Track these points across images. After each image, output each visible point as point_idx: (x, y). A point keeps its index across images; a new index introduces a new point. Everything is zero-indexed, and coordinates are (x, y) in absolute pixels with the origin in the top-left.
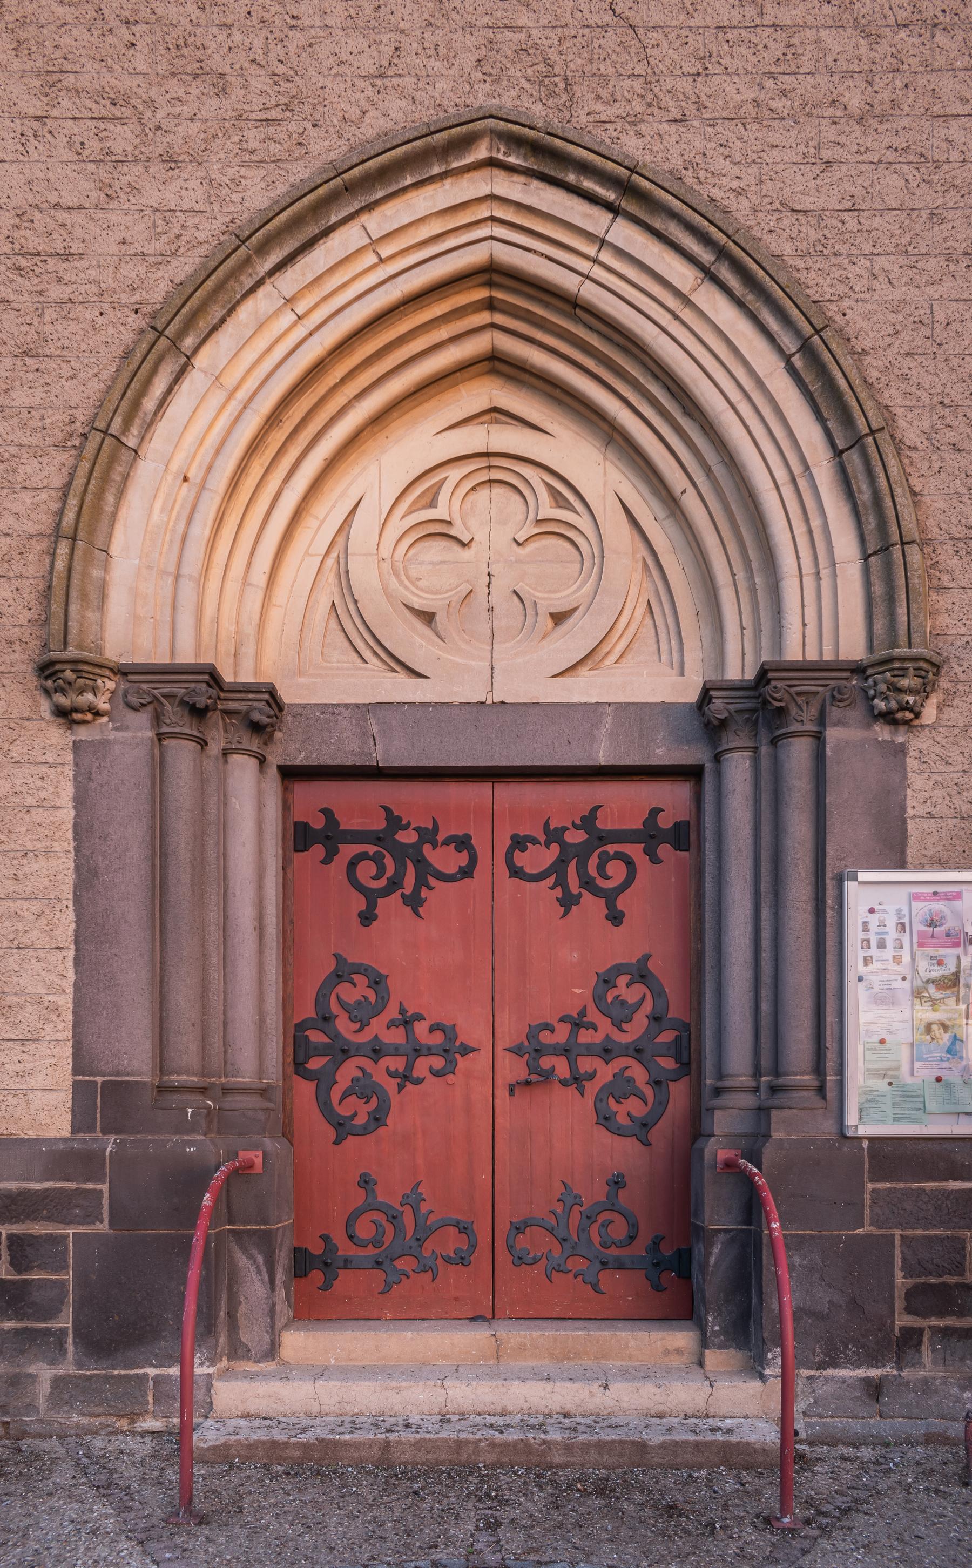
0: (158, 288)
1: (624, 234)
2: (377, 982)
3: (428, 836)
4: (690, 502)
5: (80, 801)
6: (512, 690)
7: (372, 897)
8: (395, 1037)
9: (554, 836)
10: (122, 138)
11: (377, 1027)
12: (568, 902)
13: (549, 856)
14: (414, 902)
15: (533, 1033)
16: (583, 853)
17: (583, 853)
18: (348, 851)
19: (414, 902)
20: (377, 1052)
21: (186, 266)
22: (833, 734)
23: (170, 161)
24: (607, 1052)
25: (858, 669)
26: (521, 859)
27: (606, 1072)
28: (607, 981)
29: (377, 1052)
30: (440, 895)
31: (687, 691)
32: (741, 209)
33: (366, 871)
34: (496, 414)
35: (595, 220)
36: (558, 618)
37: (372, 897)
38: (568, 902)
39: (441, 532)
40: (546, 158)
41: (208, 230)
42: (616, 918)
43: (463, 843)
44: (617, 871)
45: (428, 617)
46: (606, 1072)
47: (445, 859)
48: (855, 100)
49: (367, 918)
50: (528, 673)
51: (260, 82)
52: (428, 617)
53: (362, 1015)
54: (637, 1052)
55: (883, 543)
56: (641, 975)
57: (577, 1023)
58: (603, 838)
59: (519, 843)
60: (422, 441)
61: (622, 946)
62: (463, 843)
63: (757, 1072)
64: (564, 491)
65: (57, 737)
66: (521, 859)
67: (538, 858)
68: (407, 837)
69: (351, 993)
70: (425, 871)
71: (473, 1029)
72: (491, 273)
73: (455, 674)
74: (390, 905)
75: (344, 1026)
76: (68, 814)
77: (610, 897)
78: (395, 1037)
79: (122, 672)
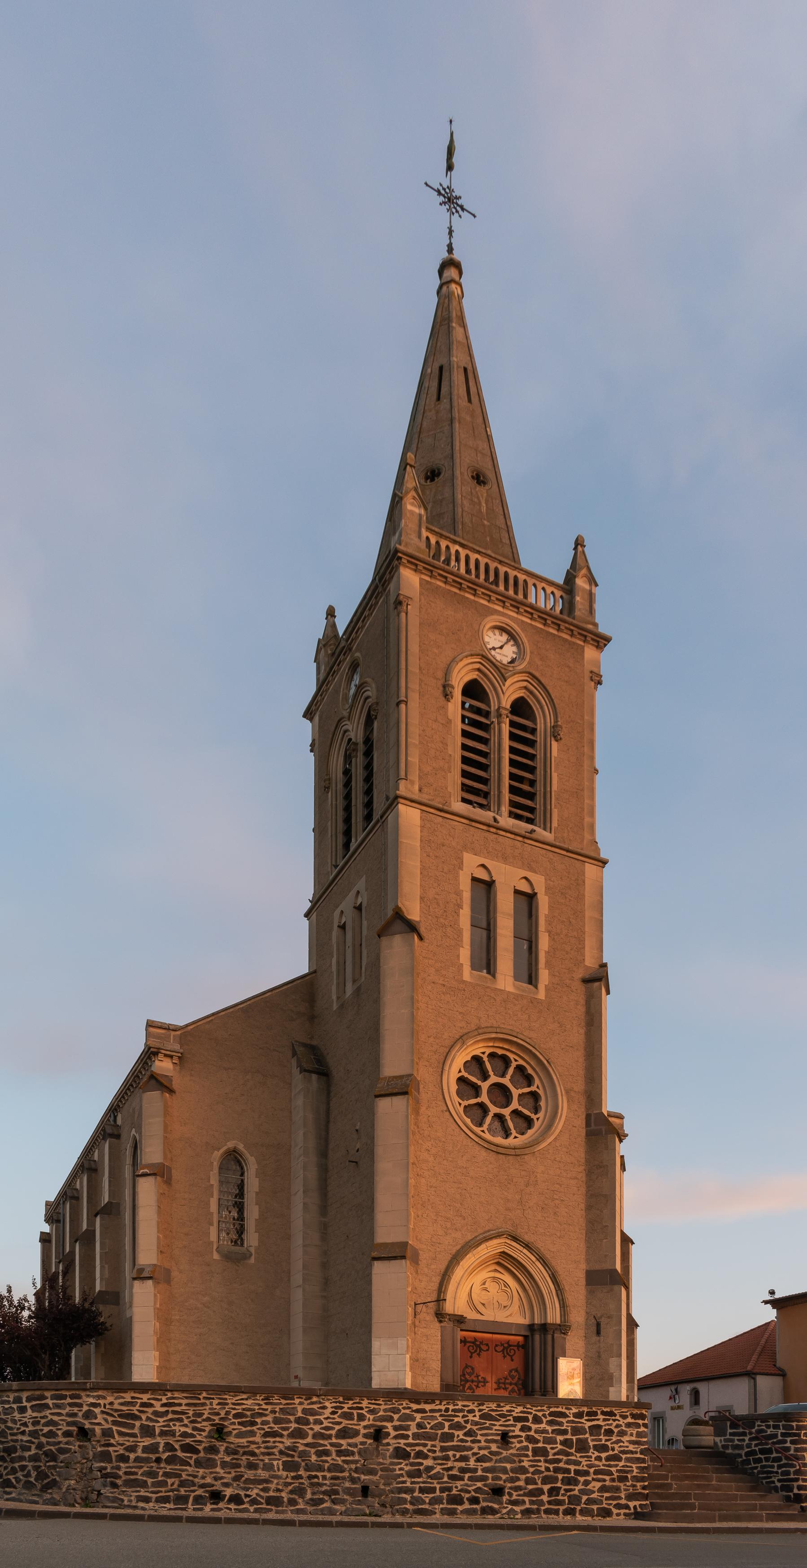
0: (454, 1251)
1: (525, 1251)
2: (473, 1369)
3: (481, 1343)
4: (530, 1291)
5: (441, 1336)
6: (498, 1319)
7: (472, 1353)
8: (475, 1379)
9: (502, 1345)
10: (449, 1225)
11: (473, 1377)
12: (504, 1357)
13: (502, 1348)
14: (479, 1355)
15: (498, 1380)
16: (507, 1348)
17: (507, 1348)
18: (468, 1344)
19: (479, 1355)
20: (472, 1381)
21: (459, 1247)
22: (556, 1335)
23: (456, 1230)
24: (511, 1384)
25: (560, 1325)
26: (497, 1348)
27: (510, 1388)
28: (511, 1371)
29: (472, 1381)
30: (483, 1354)
31: (526, 1321)
32: (542, 1249)
33: (471, 1348)
34: (496, 1271)
35: (521, 1248)
36: (505, 1307)
37: (472, 1353)
38: (504, 1357)
39: (486, 1289)
40: (515, 1239)
41: (462, 1242)
42: (512, 1360)
43: (487, 1345)
44: (512, 1352)
45: (483, 1304)
46: (510, 1388)
47: (484, 1347)
48: (558, 1234)
49: (471, 1357)
50: (501, 1317)
51: (470, 1219)
52: (483, 1304)
53: (470, 1374)
54: (516, 1384)
55: (563, 1306)
56: (516, 1371)
57: (506, 1379)
58: (510, 1346)
59: (497, 1346)
60: (485, 1274)
61: (514, 1365)
62: (487, 1345)
63: (541, 1388)
64: (506, 1285)
65: (438, 1324)
66: (497, 1348)
67: (500, 1348)
68: (478, 1343)
69: (469, 1370)
70: (481, 1350)
71: (489, 1379)
72: (504, 1252)
73: (490, 1315)
74: (475, 1355)
75: (467, 1377)
76: (440, 1338)
77: (511, 1356)
78: (475, 1379)
79: (449, 1315)
